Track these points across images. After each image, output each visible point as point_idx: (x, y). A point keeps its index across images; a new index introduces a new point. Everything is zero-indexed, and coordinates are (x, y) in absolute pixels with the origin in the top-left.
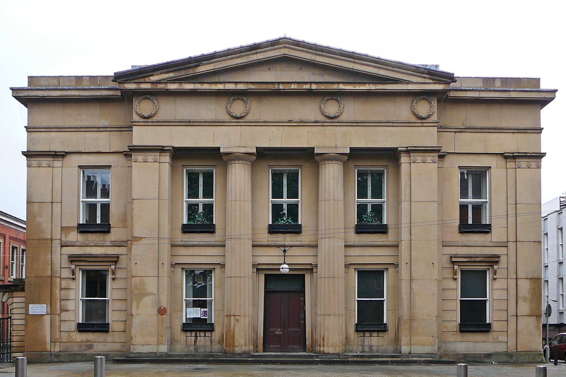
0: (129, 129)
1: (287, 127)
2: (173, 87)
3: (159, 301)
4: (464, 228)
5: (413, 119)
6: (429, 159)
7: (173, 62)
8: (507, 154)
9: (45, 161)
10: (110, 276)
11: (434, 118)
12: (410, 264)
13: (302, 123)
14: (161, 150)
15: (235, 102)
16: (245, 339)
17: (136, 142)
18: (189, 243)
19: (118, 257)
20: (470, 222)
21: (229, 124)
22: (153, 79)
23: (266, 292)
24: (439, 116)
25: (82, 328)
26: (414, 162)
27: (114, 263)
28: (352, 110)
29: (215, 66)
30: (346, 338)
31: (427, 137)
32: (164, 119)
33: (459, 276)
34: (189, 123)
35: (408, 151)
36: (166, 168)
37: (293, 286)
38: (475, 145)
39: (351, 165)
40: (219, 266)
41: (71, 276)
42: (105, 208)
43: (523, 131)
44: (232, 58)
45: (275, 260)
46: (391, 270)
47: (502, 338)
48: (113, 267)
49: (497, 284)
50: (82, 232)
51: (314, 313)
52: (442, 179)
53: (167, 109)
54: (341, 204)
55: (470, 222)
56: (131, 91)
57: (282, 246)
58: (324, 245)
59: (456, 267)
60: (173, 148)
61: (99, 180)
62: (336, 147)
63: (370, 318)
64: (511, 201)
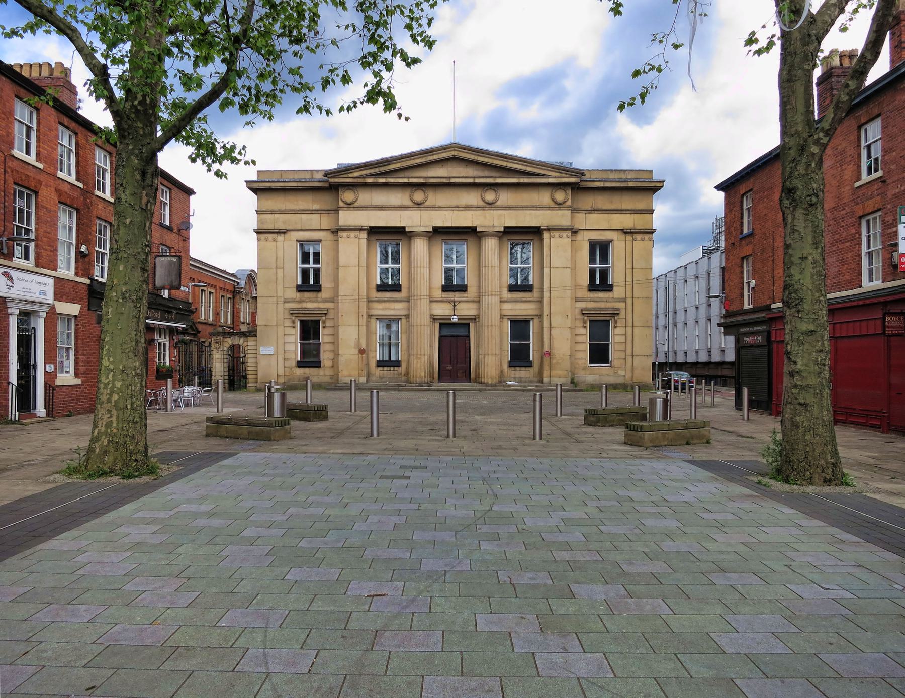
0: (336, 211)
2: (370, 180)
4: (592, 287)
5: (552, 204)
6: (565, 235)
11: (569, 203)
13: (467, 207)
14: (361, 229)
17: (341, 222)
20: (598, 282)
22: (356, 174)
23: (440, 337)
25: (300, 365)
28: (505, 197)
30: (502, 372)
31: (562, 217)
32: (363, 204)
34: (381, 208)
38: (597, 224)
39: (505, 239)
42: (317, 272)
45: (447, 312)
46: (536, 320)
47: (622, 372)
49: (617, 331)
50: (299, 291)
51: (478, 354)
52: (574, 250)
53: (365, 197)
54: (497, 269)
55: (598, 282)
58: (485, 300)
61: (311, 252)
63: (520, 356)
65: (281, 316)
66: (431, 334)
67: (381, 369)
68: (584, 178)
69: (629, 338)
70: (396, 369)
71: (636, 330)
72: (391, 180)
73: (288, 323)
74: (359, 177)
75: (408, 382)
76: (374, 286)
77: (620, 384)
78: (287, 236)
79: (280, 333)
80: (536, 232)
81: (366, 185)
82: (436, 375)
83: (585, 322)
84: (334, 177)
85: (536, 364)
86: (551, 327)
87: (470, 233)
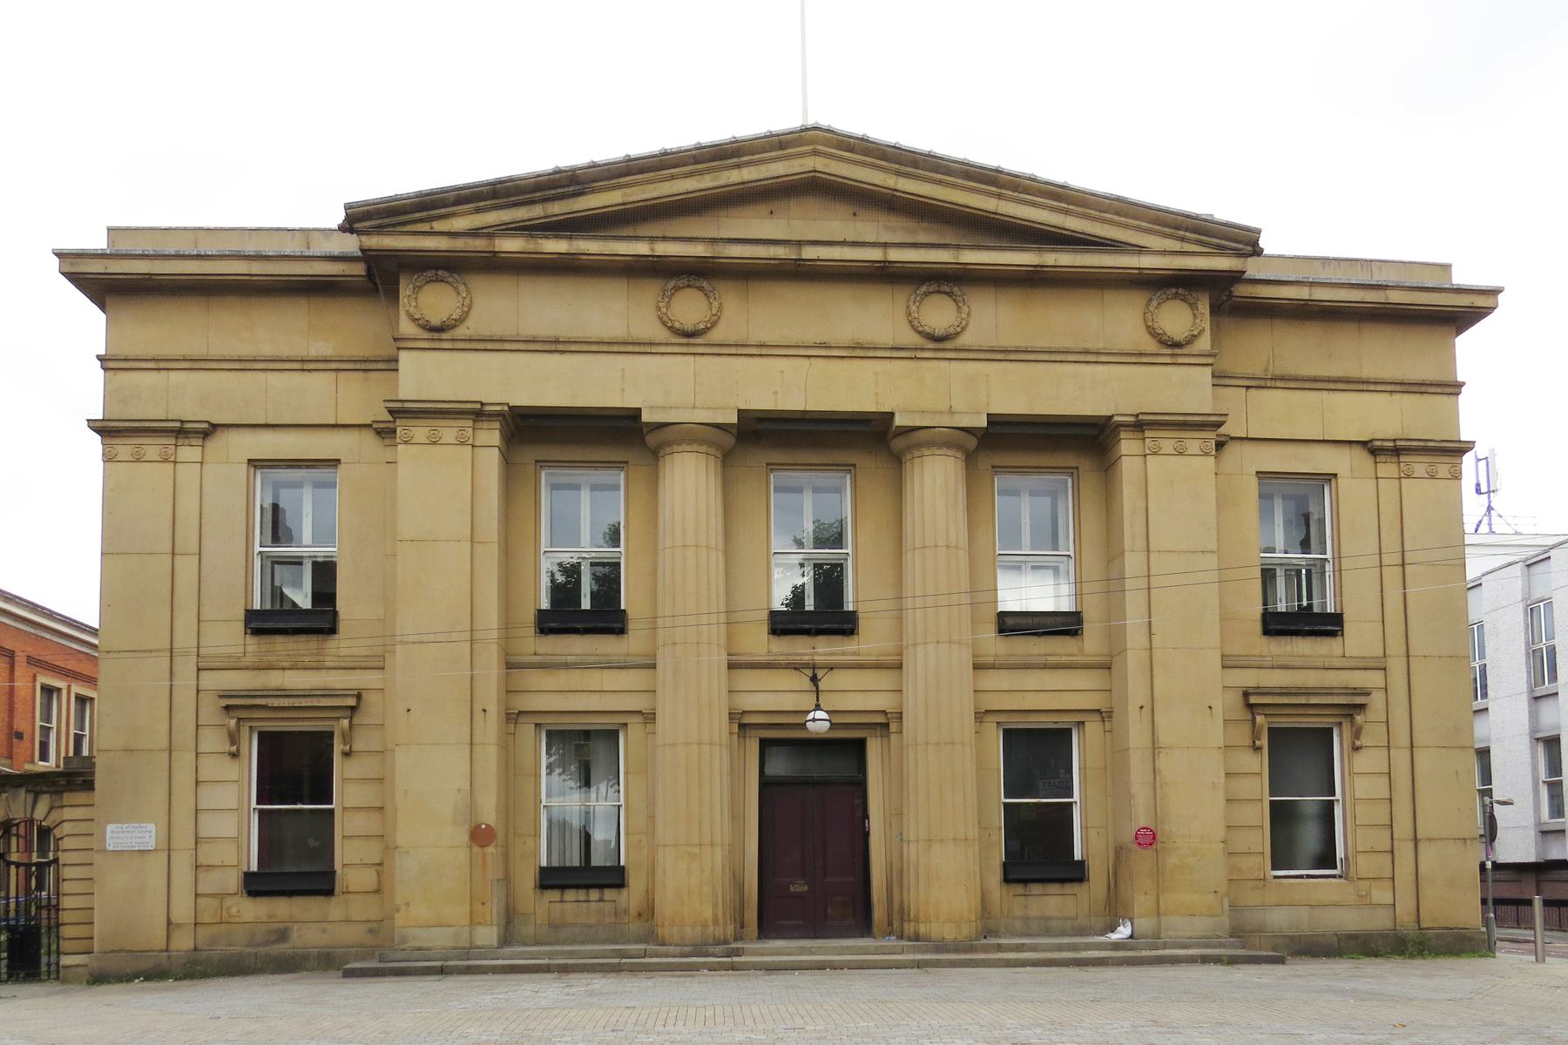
0: (391, 364)
1: (821, 361)
2: (511, 245)
3: (472, 807)
5: (1151, 345)
7: (511, 179)
8: (1378, 443)
9: (152, 448)
10: (338, 748)
11: (1204, 343)
12: (1150, 709)
13: (859, 351)
14: (478, 414)
15: (679, 294)
16: (715, 905)
18: (556, 659)
19: (359, 697)
21: (663, 349)
22: (460, 224)
23: (766, 784)
24: (1215, 340)
25: (256, 885)
26: (1155, 453)
27: (348, 713)
28: (990, 318)
29: (625, 195)
30: (983, 900)
31: (1186, 388)
32: (485, 332)
33: (1264, 742)
34: (555, 345)
35: (1140, 425)
36: (491, 460)
37: (835, 768)
40: (638, 719)
41: (227, 747)
43: (1416, 389)
44: (673, 177)
45: (788, 703)
46: (1093, 727)
47: (1382, 895)
48: (346, 722)
49: (1362, 762)
50: (257, 632)
53: (497, 306)
54: (963, 557)
56: (395, 257)
57: (806, 666)
59: (1259, 719)
60: (511, 408)
62: (951, 412)
64: (1391, 558)
65: (185, 717)
66: (736, 775)
67: (554, 895)
68: (1253, 268)
69: (1402, 783)
70: (609, 894)
71: (1422, 758)
72: (590, 246)
73: (214, 741)
74: (474, 233)
75: (650, 936)
76: (530, 617)
77: (1382, 936)
78: (214, 444)
79: (184, 778)
80: (1086, 442)
81: (495, 265)
82: (752, 915)
83: (1255, 735)
84: (380, 230)
85: (1098, 873)
86: (1155, 748)
87: (867, 439)
